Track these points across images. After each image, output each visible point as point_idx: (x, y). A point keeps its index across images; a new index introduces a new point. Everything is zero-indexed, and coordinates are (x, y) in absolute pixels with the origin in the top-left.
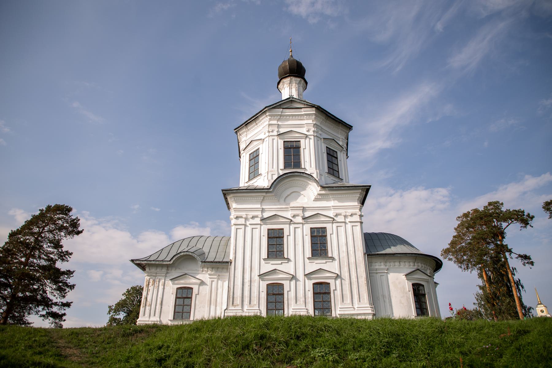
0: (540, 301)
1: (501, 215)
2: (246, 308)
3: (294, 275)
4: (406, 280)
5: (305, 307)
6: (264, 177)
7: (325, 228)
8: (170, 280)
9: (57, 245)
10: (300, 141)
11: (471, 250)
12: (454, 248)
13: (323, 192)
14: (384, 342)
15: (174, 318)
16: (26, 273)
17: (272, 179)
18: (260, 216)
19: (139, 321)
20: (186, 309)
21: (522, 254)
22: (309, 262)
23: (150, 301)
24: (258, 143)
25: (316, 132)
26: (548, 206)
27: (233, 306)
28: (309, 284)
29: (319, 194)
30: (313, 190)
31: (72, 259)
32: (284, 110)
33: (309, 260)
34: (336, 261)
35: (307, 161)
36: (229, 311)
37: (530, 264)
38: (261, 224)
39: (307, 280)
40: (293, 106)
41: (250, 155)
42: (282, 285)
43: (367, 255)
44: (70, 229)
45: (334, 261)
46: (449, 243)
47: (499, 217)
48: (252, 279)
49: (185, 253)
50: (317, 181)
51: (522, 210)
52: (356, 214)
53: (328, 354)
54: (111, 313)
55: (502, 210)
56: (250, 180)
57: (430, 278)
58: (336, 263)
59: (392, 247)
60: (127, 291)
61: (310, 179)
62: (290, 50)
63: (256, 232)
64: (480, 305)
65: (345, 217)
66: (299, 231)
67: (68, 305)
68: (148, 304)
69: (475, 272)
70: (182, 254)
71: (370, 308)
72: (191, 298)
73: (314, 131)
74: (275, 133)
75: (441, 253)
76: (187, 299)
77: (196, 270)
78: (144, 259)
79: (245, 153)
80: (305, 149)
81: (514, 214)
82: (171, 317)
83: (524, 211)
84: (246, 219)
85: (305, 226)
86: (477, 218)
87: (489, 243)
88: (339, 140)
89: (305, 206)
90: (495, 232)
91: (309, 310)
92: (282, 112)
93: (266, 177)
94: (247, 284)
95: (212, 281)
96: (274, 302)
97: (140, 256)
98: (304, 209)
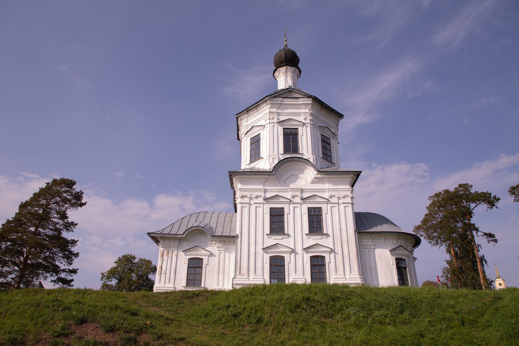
0: (499, 275)
1: (470, 196)
2: (251, 277)
3: (294, 249)
4: (391, 255)
5: (304, 277)
7: (321, 208)
9: (63, 216)
10: (298, 128)
11: (441, 228)
12: (426, 226)
13: (319, 176)
14: (398, 304)
16: (39, 242)
17: (273, 162)
18: (263, 196)
19: (156, 287)
20: (197, 277)
21: (487, 232)
22: (307, 238)
23: (165, 269)
24: (260, 128)
25: (313, 121)
26: (513, 190)
27: (240, 275)
28: (307, 258)
29: (315, 178)
30: (310, 173)
31: (76, 229)
32: (283, 99)
33: (307, 236)
34: (331, 238)
35: (305, 147)
36: (237, 279)
37: (494, 241)
38: (263, 203)
39: (305, 254)
40: (292, 96)
41: (251, 139)
43: (358, 233)
44: (74, 201)
45: (329, 237)
46: (422, 220)
47: (468, 198)
48: (256, 252)
49: (196, 228)
50: (314, 166)
51: (489, 192)
52: (348, 196)
53: (358, 312)
54: (103, 279)
55: (471, 191)
56: (251, 162)
57: (410, 254)
58: (330, 239)
59: (378, 226)
60: (118, 259)
61: (307, 163)
62: (285, 40)
63: (260, 210)
64: (447, 278)
65: (339, 198)
66: (298, 210)
67: (74, 271)
68: (163, 272)
69: (444, 248)
70: (194, 228)
71: (360, 279)
72: (202, 267)
73: (310, 120)
74: (275, 120)
75: (413, 229)
76: (198, 269)
77: (206, 243)
78: (159, 232)
79: (246, 137)
80: (303, 135)
81: (482, 196)
82: (184, 283)
83: (491, 193)
84: (251, 198)
86: (448, 199)
87: (457, 222)
88: (332, 128)
89: (302, 188)
90: (464, 212)
92: (281, 101)
93: (268, 161)
94: (252, 256)
95: (220, 253)
96: (276, 272)
97: (155, 229)
98: (302, 191)
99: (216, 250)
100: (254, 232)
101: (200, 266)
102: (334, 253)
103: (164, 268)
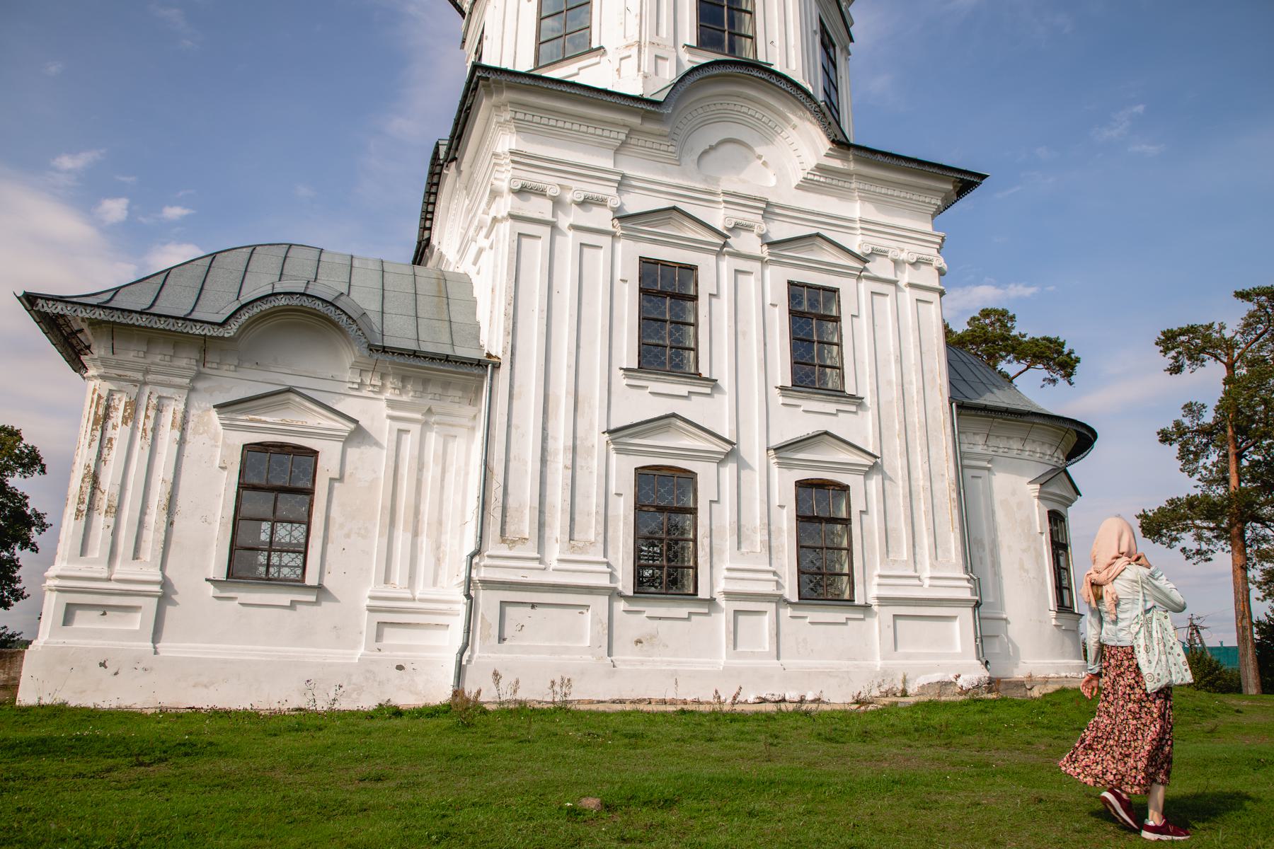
2: (554, 552)
4: (1036, 501)
5: (770, 565)
6: (621, 59)
8: (215, 407)
13: (837, 164)
15: (230, 574)
22: (783, 404)
23: (116, 490)
27: (504, 541)
28: (784, 483)
29: (820, 169)
36: (487, 561)
39: (775, 470)
42: (691, 476)
43: (958, 407)
45: (862, 410)
48: (578, 442)
49: (295, 302)
68: (103, 502)
70: (282, 302)
71: (965, 583)
72: (310, 492)
77: (333, 379)
85: (769, 271)
89: (772, 199)
91: (782, 576)
95: (401, 432)
98: (769, 210)
99: (385, 416)
100: (569, 353)
101: (300, 485)
102: (736, 465)
103: (112, 484)
